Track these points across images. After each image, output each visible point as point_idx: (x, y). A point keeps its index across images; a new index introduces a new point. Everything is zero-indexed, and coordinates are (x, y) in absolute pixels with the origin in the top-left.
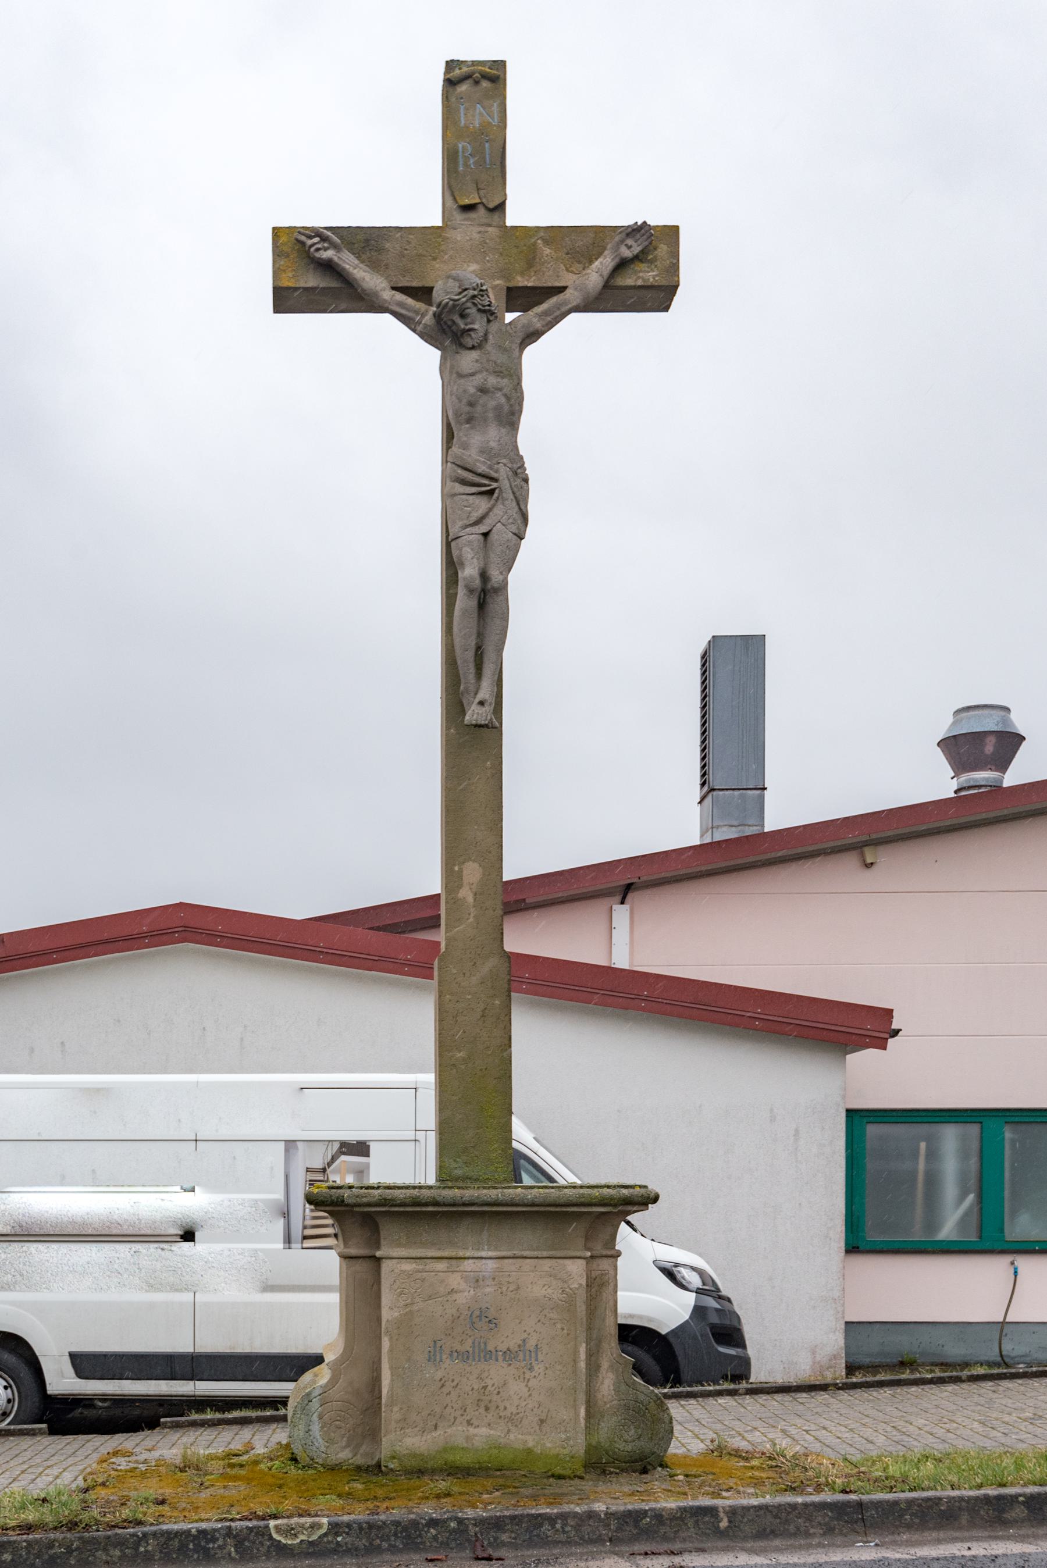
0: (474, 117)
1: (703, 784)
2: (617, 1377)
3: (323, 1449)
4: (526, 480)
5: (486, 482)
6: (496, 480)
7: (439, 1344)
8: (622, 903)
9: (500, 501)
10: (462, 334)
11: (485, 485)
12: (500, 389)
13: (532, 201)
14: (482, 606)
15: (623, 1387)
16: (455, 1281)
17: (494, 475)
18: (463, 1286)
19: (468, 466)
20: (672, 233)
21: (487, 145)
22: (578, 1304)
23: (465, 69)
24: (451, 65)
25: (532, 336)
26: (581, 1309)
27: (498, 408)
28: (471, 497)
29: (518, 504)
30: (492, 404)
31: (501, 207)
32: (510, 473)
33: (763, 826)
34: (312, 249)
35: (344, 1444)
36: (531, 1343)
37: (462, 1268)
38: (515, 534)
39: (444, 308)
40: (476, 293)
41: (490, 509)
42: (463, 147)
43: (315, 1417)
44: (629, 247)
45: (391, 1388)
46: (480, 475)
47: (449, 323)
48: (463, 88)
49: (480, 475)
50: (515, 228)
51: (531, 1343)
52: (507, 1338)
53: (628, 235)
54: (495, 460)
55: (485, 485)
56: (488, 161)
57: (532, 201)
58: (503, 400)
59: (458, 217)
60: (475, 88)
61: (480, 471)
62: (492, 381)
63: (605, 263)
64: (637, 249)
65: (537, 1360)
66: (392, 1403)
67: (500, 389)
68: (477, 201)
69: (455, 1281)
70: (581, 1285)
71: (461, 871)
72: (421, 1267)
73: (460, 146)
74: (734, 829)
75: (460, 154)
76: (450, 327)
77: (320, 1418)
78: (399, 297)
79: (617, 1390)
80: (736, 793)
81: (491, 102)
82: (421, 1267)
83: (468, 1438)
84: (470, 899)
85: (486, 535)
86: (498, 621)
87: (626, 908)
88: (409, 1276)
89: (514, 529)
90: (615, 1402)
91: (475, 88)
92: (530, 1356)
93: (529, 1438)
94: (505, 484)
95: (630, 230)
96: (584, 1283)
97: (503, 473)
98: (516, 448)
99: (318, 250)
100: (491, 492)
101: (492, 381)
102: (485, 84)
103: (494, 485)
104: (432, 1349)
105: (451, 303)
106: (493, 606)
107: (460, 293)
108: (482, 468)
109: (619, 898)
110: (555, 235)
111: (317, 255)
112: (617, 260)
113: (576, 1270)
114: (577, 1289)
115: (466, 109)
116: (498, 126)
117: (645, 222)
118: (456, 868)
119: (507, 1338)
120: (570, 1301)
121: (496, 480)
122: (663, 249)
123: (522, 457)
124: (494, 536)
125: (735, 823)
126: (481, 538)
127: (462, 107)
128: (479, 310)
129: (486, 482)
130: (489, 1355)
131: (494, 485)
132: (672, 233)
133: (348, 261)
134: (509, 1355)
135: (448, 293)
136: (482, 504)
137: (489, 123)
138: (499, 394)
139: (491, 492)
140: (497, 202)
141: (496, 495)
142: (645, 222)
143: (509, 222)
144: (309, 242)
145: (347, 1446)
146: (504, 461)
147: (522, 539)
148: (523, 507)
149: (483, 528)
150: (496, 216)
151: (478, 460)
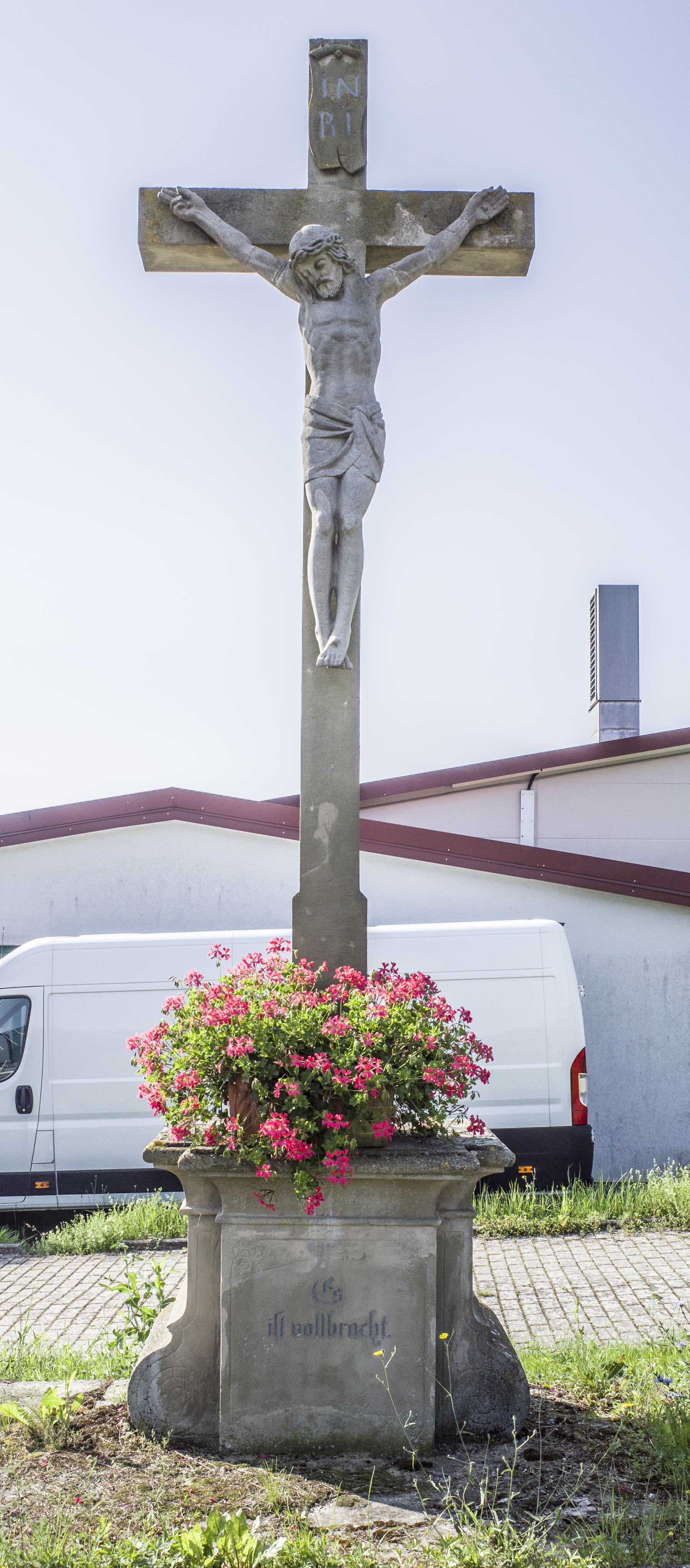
0: (338, 89)
1: (592, 697)
2: (471, 1344)
3: (162, 1417)
4: (382, 426)
5: (341, 426)
6: (351, 425)
7: (279, 1317)
8: (529, 788)
9: (354, 445)
10: (318, 285)
11: (339, 429)
12: (355, 338)
13: (392, 165)
14: (336, 548)
15: (478, 1355)
16: (298, 1248)
17: (348, 419)
18: (306, 1254)
19: (322, 411)
20: (526, 200)
21: (348, 115)
22: (428, 1275)
23: (327, 45)
24: (313, 43)
25: (393, 290)
26: (431, 1278)
27: (354, 355)
28: (325, 441)
29: (373, 448)
30: (348, 351)
31: (360, 173)
32: (365, 419)
33: (638, 730)
34: (175, 207)
35: (184, 1412)
36: (378, 1319)
37: (304, 1236)
38: (368, 477)
39: (298, 259)
40: (330, 244)
41: (345, 453)
42: (325, 117)
43: (154, 1383)
44: (485, 210)
45: (229, 1364)
46: (333, 419)
47: (305, 274)
48: (328, 61)
49: (333, 419)
50: (375, 192)
51: (378, 1319)
52: (353, 1312)
53: (484, 198)
54: (349, 406)
55: (339, 429)
56: (349, 130)
57: (392, 165)
58: (359, 348)
59: (322, 179)
60: (339, 64)
61: (333, 415)
62: (348, 330)
63: (461, 224)
64: (493, 213)
65: (383, 1334)
66: (229, 1380)
67: (355, 338)
68: (338, 165)
69: (298, 1248)
70: (431, 1255)
71: (316, 812)
72: (261, 1234)
73: (322, 115)
74: (616, 731)
75: (322, 122)
76: (306, 278)
77: (159, 1383)
78: (259, 251)
79: (472, 1360)
80: (618, 704)
81: (353, 76)
82: (261, 1234)
83: (311, 1418)
84: (326, 841)
85: (340, 478)
86: (351, 563)
87: (532, 792)
88: (249, 1243)
89: (368, 472)
90: (470, 1371)
91: (339, 64)
92: (377, 1330)
93: (376, 1418)
94: (357, 428)
95: (486, 193)
96: (435, 1253)
97: (357, 418)
98: (373, 397)
99: (181, 207)
100: (345, 437)
101: (348, 330)
102: (347, 60)
103: (349, 429)
104: (272, 1322)
105: (305, 253)
106: (347, 549)
107: (314, 244)
108: (335, 412)
109: (526, 785)
110: (417, 201)
111: (181, 212)
112: (473, 222)
113: (425, 1239)
114: (427, 1259)
115: (328, 82)
116: (359, 98)
117: (500, 187)
118: (312, 809)
119: (353, 1312)
120: (420, 1267)
121: (351, 425)
122: (519, 214)
123: (378, 404)
124: (348, 479)
125: (617, 727)
126: (335, 481)
127: (325, 81)
128: (333, 261)
129: (341, 426)
130: (334, 1330)
131: (349, 429)
132: (526, 200)
133: (210, 219)
134: (355, 1330)
135: (302, 245)
136: (336, 446)
137: (352, 96)
138: (353, 343)
139: (345, 437)
140: (357, 167)
141: (350, 439)
142: (500, 187)
143: (369, 187)
144: (174, 200)
145: (188, 1413)
146: (359, 407)
147: (375, 482)
148: (377, 451)
149: (338, 471)
150: (357, 180)
151: (333, 405)
